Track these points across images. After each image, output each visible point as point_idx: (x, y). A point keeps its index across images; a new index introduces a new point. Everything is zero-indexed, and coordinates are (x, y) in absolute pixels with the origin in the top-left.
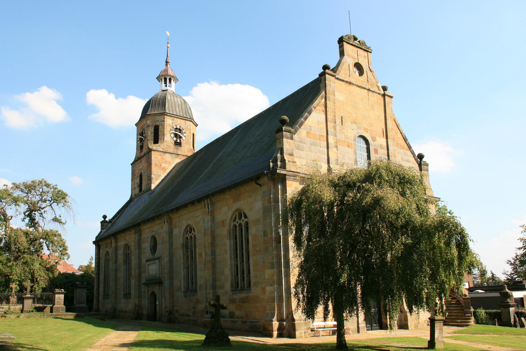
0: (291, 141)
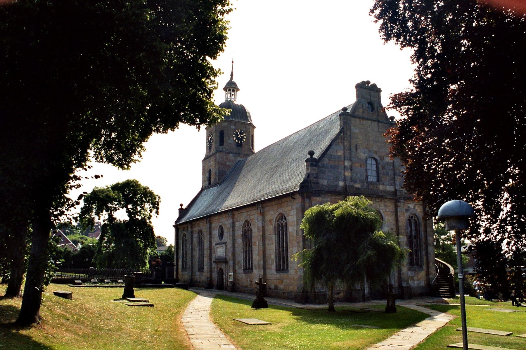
0: (316, 168)
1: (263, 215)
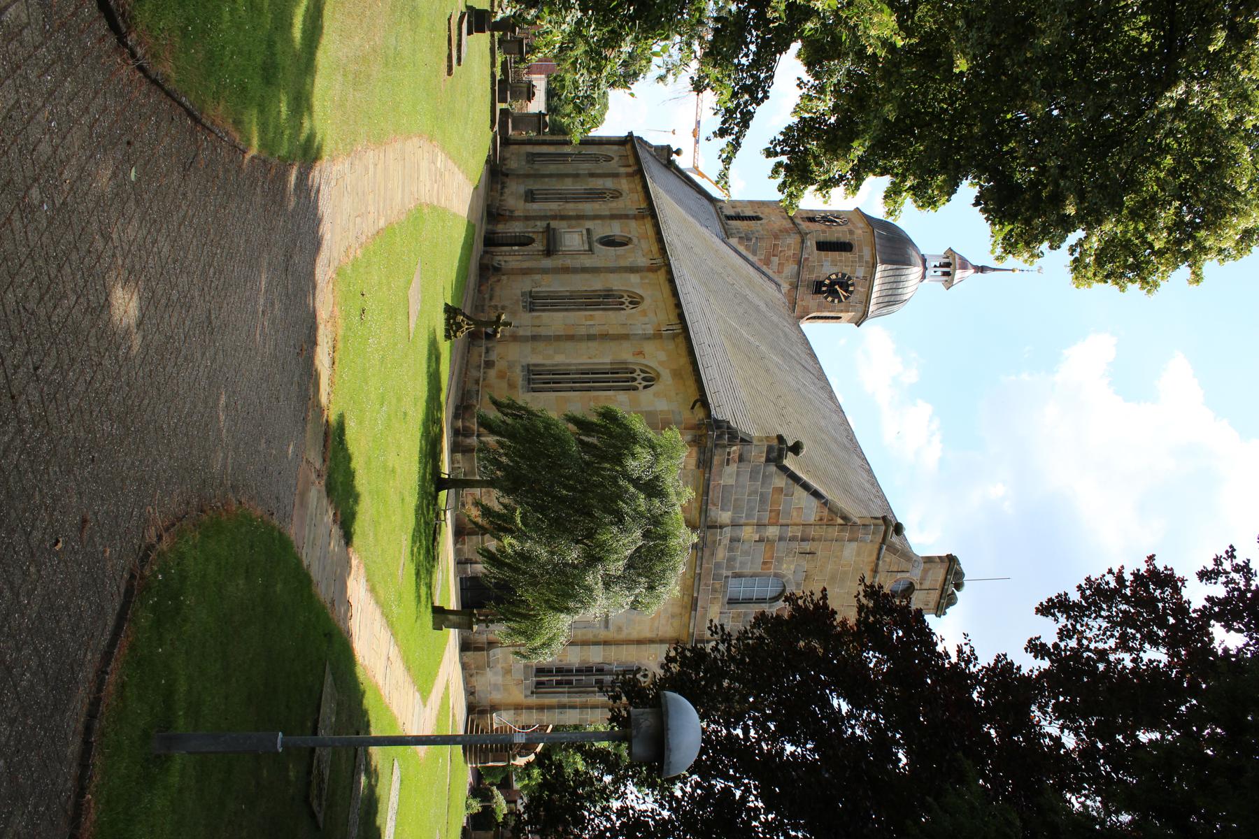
0: (763, 459)
1: (657, 336)
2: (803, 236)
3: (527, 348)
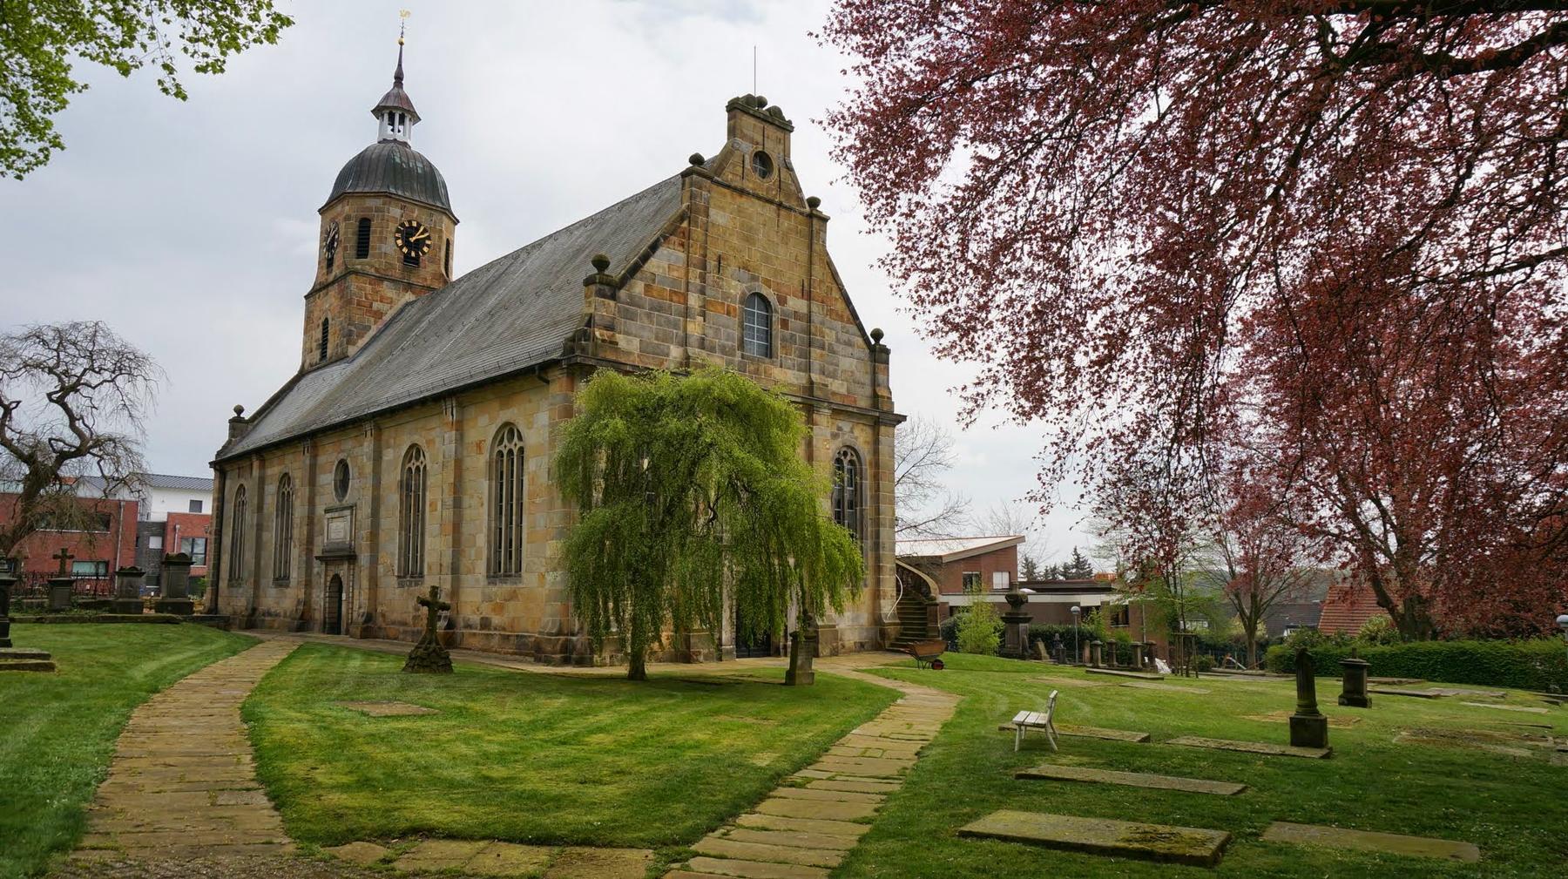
0: (612, 303)
1: (459, 427)
2: (349, 272)
3: (467, 580)
